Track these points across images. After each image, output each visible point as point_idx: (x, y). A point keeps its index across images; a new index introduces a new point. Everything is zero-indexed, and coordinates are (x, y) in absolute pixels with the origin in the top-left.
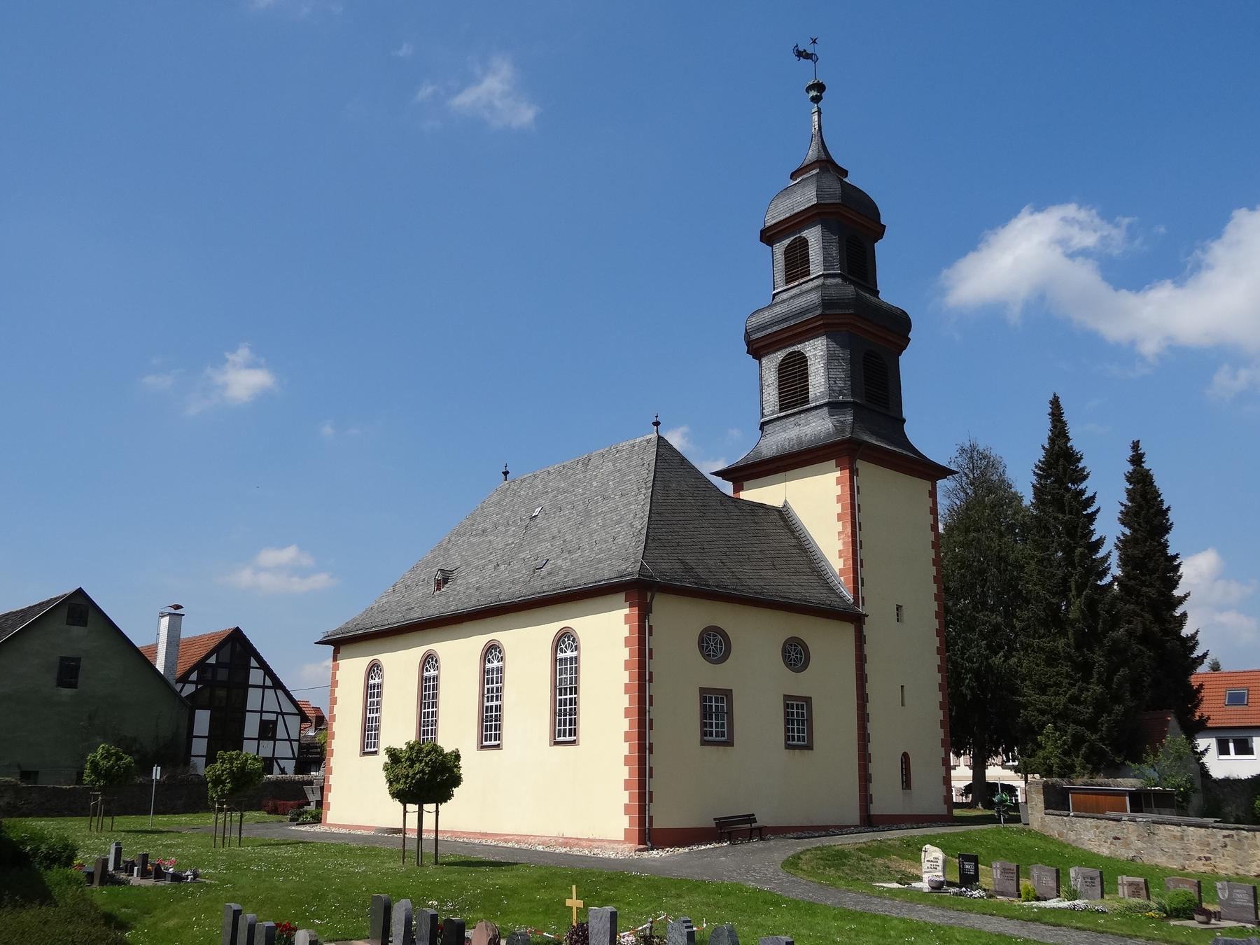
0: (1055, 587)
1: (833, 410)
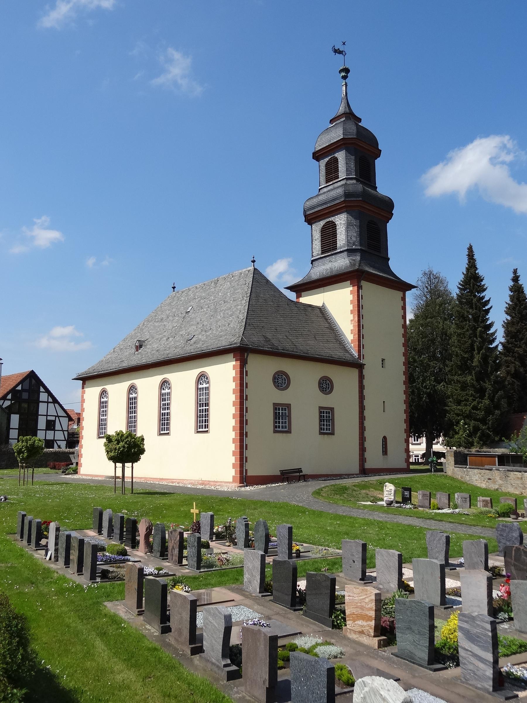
0: (466, 349)
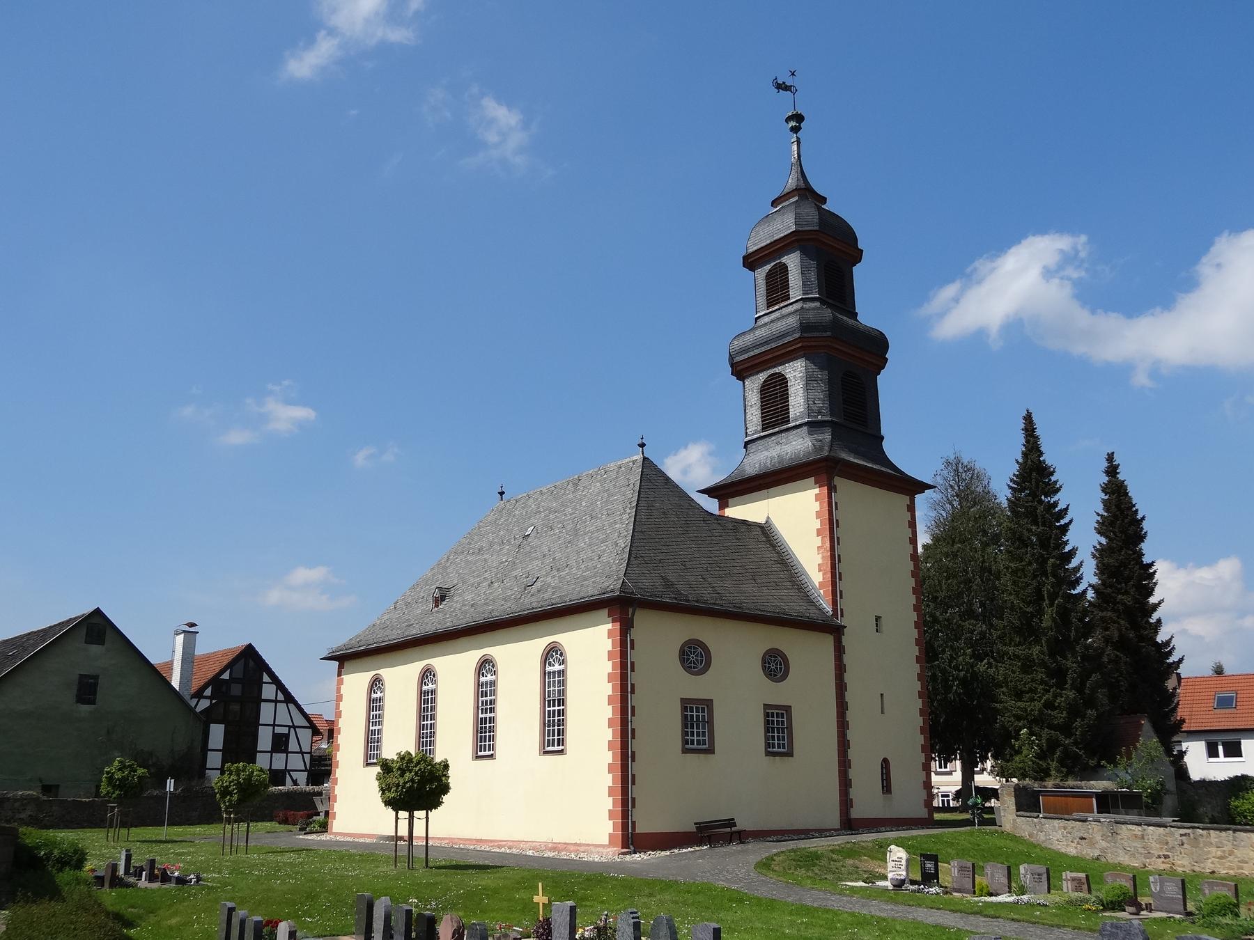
1: (813, 429)
